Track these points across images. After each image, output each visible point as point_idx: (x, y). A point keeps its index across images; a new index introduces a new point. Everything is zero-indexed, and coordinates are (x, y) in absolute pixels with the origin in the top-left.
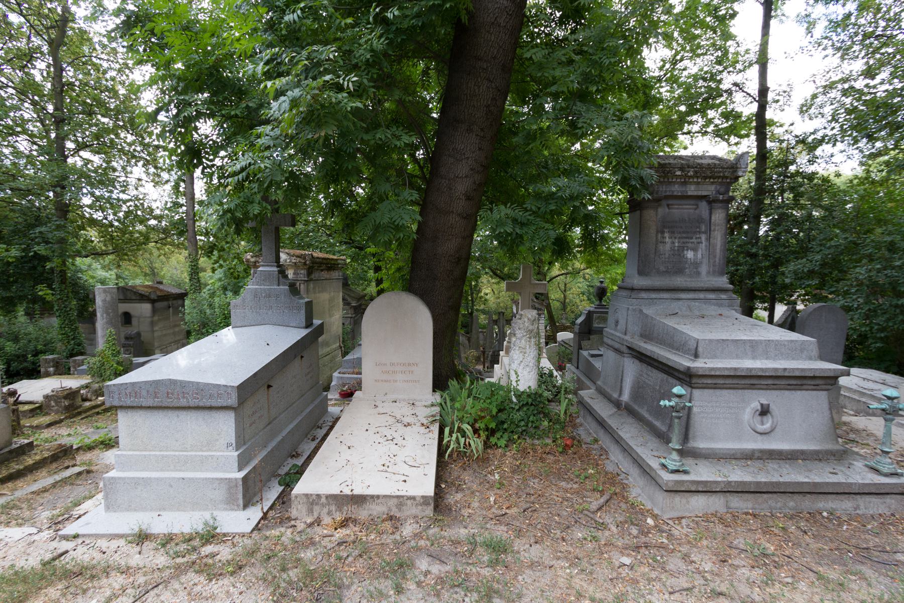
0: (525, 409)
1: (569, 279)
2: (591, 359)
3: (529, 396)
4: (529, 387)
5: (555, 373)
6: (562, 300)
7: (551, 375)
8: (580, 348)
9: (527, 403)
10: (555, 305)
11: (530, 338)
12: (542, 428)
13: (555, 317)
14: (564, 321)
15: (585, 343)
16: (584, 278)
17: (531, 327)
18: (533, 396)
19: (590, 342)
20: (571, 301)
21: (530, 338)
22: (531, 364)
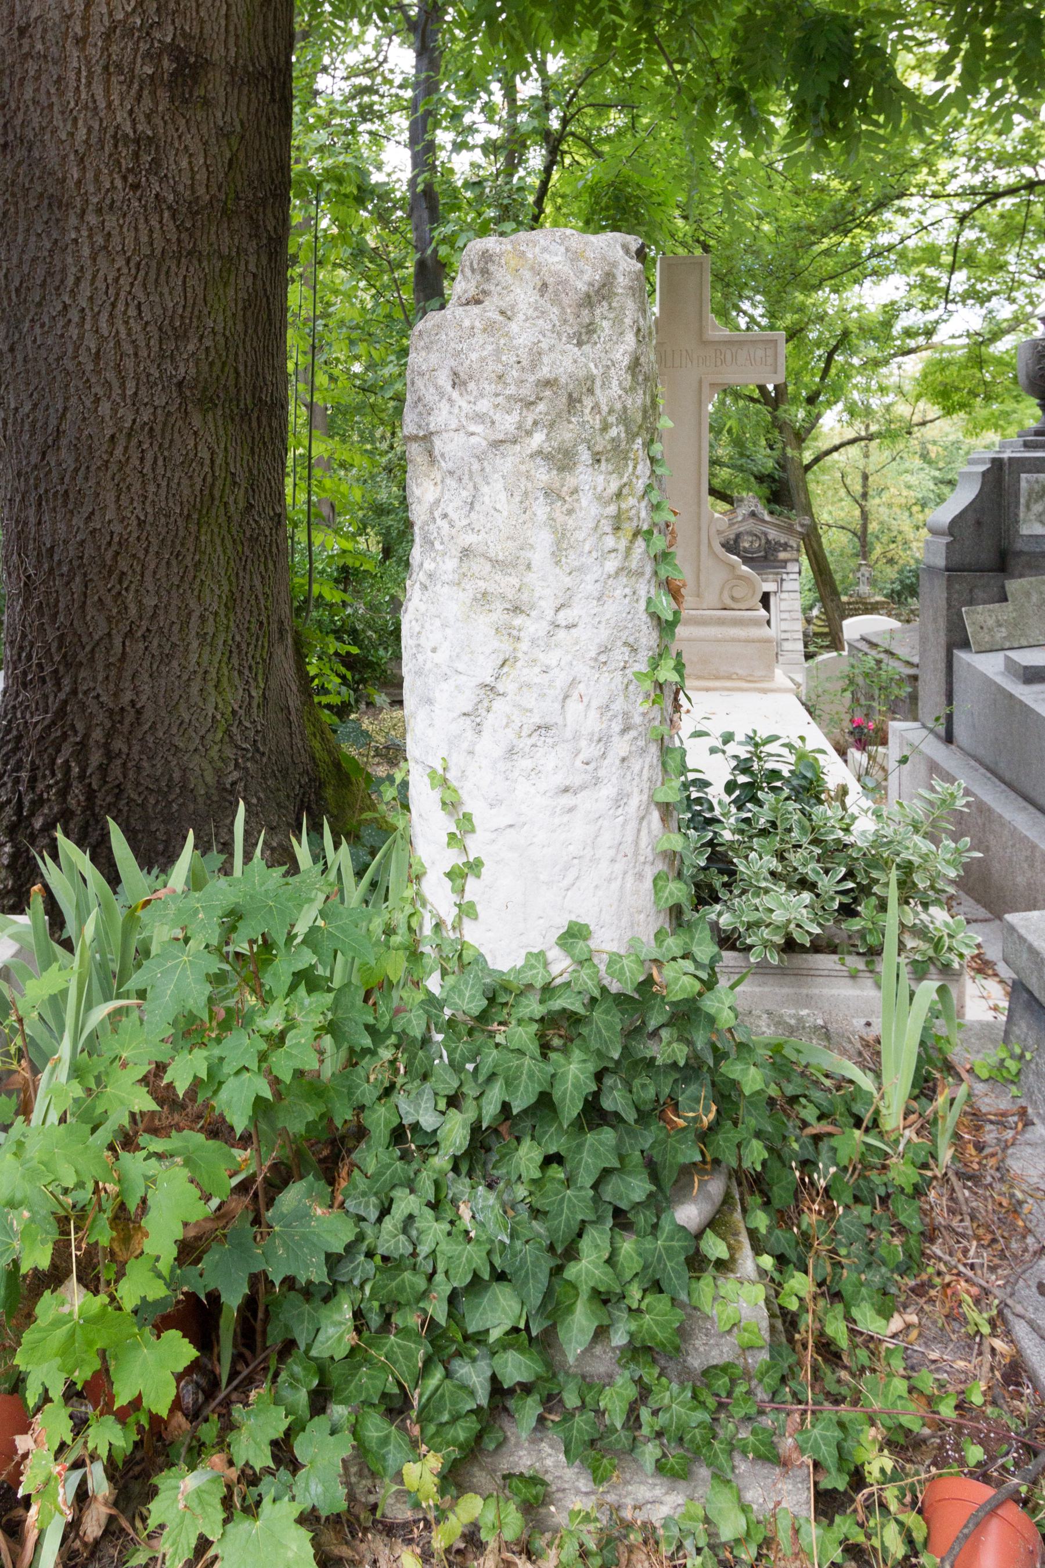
0: (527, 1156)
1: (880, 454)
2: (1026, 694)
3: (559, 1028)
4: (574, 935)
5: (836, 772)
6: (857, 525)
7: (808, 788)
8: (959, 639)
9: (545, 1103)
10: (835, 542)
11: (562, 460)
12: (707, 1352)
13: (837, 577)
14: (864, 589)
15: (979, 618)
16: (924, 456)
17: (565, 362)
18: (606, 1025)
19: (1005, 611)
20: (885, 528)
21: (562, 460)
22: (582, 718)
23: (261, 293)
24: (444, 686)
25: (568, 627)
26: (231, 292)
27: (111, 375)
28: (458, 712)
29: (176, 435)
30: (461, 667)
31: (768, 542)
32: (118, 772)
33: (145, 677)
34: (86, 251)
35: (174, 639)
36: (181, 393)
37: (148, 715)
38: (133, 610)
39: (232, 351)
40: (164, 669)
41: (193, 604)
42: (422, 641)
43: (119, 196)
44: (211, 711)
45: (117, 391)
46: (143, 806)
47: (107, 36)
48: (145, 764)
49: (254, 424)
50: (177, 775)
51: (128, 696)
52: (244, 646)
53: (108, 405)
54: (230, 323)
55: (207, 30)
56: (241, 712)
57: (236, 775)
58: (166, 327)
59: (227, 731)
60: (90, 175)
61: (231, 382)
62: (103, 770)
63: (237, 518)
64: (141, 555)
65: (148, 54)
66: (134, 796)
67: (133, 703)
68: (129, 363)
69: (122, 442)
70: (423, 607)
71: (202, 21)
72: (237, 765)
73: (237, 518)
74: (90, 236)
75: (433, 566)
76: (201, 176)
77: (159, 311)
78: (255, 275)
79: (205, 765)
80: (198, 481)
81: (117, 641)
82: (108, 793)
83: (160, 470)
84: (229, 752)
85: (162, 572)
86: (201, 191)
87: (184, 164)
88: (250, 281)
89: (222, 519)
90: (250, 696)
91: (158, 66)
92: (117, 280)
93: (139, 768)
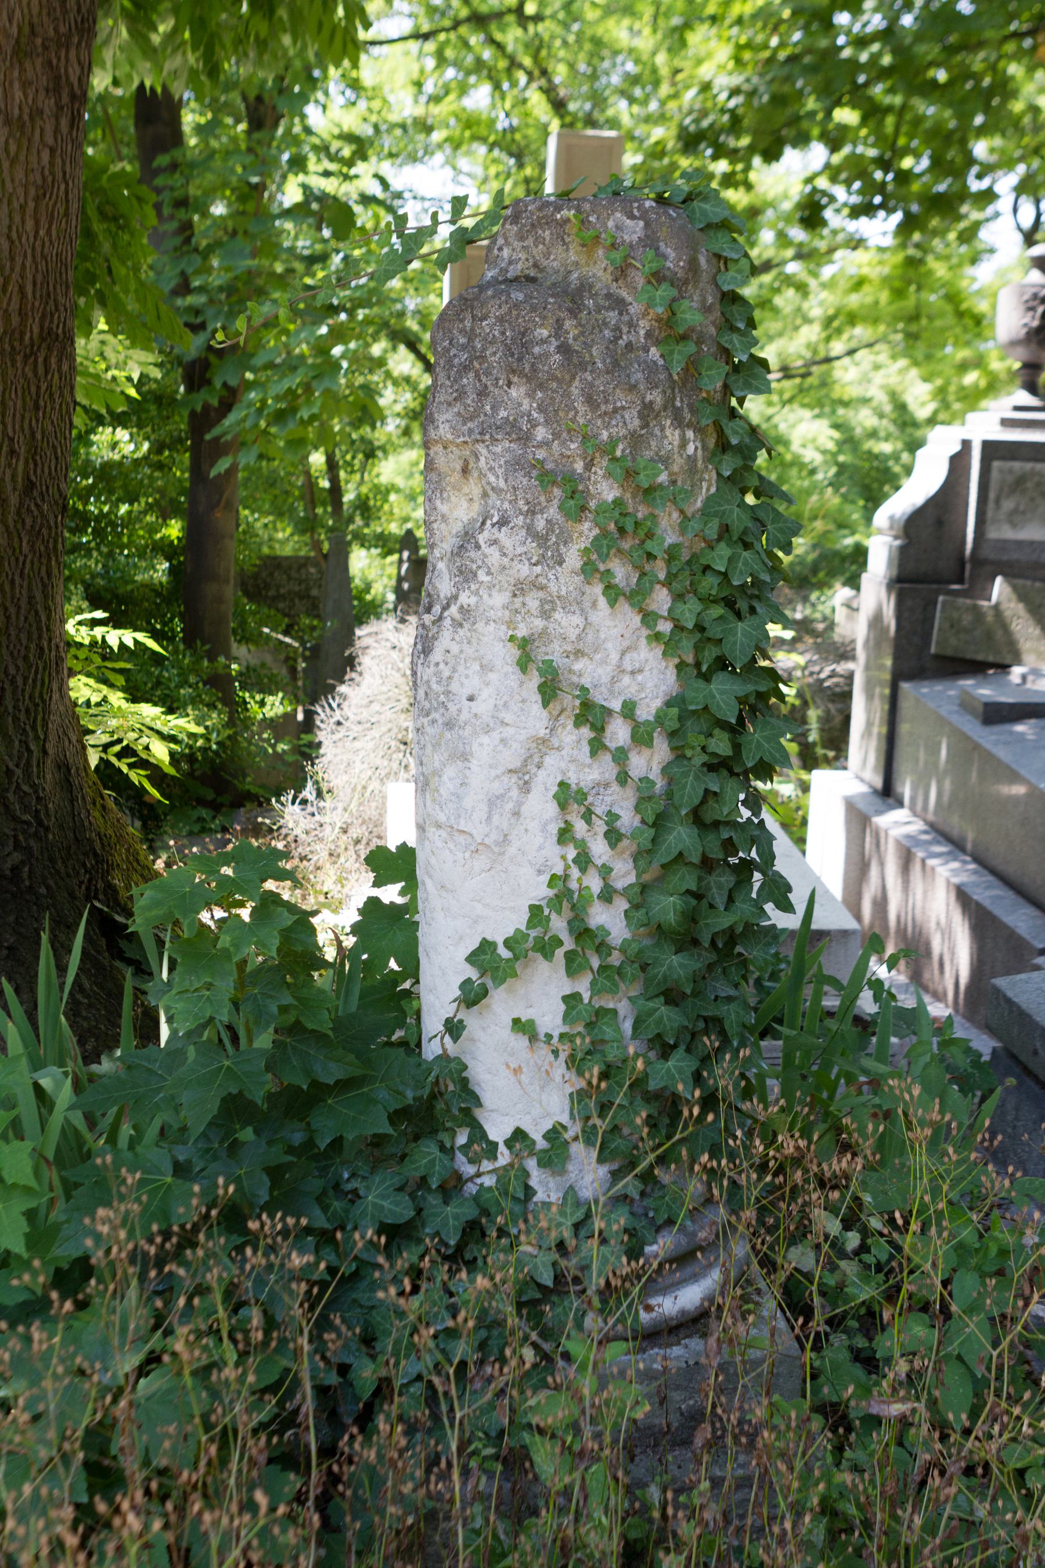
23: (59, 175)
24: (485, 739)
25: (633, 673)
26: (20, 175)
28: (501, 769)
30: (508, 717)
39: (19, 260)
42: (454, 687)
49: (41, 370)
52: (20, 680)
54: (17, 218)
56: (18, 772)
57: (17, 857)
61: (15, 305)
70: (455, 648)
72: (17, 845)
75: (473, 600)
78: (53, 151)
88: (46, 155)
90: (28, 750)
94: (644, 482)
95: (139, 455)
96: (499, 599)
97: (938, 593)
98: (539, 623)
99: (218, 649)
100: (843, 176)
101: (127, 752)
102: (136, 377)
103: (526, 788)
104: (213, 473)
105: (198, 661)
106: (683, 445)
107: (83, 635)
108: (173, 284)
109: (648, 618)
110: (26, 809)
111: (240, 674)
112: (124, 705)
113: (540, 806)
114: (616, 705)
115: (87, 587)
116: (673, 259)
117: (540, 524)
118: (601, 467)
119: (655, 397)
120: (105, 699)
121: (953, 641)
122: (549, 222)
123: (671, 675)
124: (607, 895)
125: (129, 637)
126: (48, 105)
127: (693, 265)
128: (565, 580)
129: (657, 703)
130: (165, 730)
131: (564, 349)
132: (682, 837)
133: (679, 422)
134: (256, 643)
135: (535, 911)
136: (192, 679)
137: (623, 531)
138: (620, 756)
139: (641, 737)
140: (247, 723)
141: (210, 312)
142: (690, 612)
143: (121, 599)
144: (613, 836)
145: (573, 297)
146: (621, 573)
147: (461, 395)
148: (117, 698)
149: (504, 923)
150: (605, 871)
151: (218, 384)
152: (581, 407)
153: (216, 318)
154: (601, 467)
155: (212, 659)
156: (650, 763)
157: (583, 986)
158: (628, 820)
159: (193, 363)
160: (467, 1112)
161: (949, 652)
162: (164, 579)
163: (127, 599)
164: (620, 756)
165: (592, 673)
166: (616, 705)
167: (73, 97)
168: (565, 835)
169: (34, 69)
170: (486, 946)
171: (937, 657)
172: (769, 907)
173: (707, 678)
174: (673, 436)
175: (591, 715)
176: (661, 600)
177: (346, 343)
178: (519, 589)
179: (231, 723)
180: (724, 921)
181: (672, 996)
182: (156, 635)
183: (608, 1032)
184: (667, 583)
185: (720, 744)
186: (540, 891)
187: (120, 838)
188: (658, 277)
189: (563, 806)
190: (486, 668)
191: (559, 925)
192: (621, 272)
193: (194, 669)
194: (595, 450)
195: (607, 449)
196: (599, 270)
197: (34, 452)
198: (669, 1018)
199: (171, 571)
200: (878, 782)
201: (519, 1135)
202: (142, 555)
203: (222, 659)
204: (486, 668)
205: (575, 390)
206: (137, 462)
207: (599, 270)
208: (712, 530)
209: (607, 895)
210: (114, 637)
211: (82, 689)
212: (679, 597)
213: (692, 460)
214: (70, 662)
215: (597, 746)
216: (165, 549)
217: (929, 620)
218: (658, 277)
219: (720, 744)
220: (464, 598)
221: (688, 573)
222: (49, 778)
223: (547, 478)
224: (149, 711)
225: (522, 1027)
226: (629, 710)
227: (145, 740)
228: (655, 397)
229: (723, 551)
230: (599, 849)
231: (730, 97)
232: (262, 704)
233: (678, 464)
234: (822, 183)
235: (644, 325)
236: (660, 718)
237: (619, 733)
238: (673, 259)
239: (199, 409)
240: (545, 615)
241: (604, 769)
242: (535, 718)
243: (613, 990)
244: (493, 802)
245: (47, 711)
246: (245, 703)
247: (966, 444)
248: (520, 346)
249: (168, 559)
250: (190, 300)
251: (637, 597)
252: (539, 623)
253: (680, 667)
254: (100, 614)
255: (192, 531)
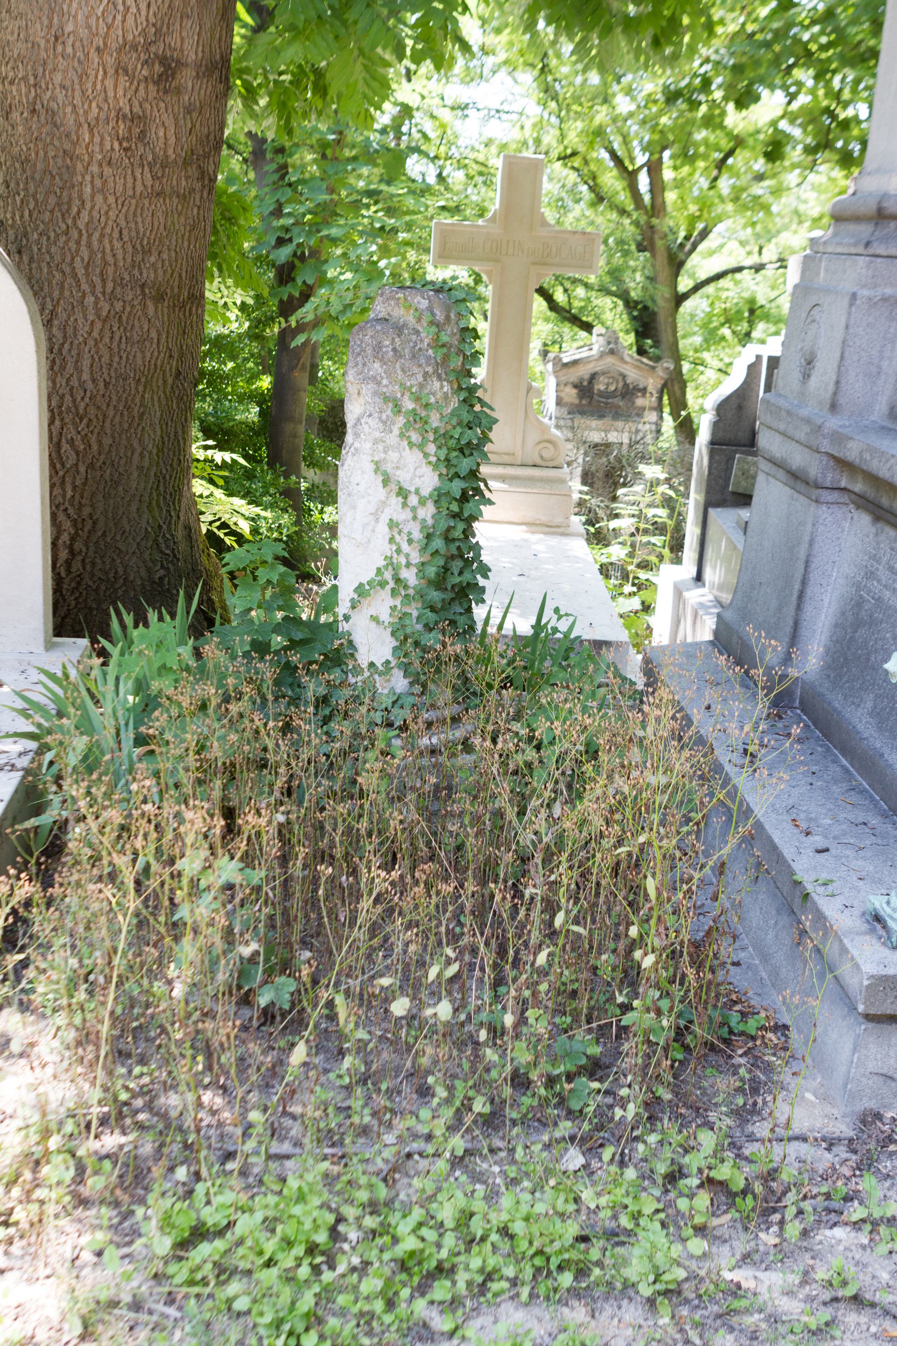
26: (182, 220)
27: (97, 280)
29: (136, 323)
31: (626, 385)
32: (80, 565)
33: (100, 497)
34: (88, 190)
35: (121, 470)
36: (143, 292)
37: (101, 525)
38: (95, 447)
40: (113, 492)
41: (136, 444)
43: (116, 155)
44: (144, 525)
45: (99, 289)
46: (96, 591)
47: (119, 51)
48: (98, 560)
50: (121, 571)
51: (86, 511)
53: (92, 299)
55: (185, 46)
57: (162, 572)
58: (138, 246)
59: (156, 541)
60: (97, 139)
62: (68, 563)
63: (170, 381)
64: (104, 407)
65: (146, 62)
66: (90, 583)
67: (91, 516)
68: (110, 270)
69: (98, 325)
71: (182, 39)
72: (162, 567)
73: (170, 381)
74: (92, 182)
76: (172, 141)
77: (133, 234)
79: (141, 564)
80: (148, 355)
81: (82, 469)
82: (72, 580)
83: (123, 346)
84: (157, 556)
85: (117, 419)
86: (170, 151)
87: (161, 134)
88: (195, 211)
89: (161, 382)
91: (151, 70)
92: (107, 213)
93: (93, 564)
94: (424, 402)
95: (241, 331)
96: (368, 446)
97: (736, 452)
98: (383, 456)
99: (291, 469)
100: (799, 121)
101: (224, 525)
102: (239, 303)
103: (377, 520)
104: (293, 345)
105: (277, 478)
106: (442, 387)
107: (201, 455)
108: (271, 208)
109: (426, 455)
110: (168, 547)
111: (308, 489)
112: (224, 497)
113: (383, 529)
114: (413, 489)
115: (202, 422)
116: (440, 316)
117: (384, 417)
118: (406, 397)
119: (430, 369)
120: (211, 495)
121: (744, 483)
122: (393, 298)
123: (436, 478)
124: (408, 565)
125: (228, 456)
126: (198, 186)
127: (448, 318)
128: (393, 438)
129: (430, 489)
130: (247, 514)
131: (394, 350)
132: (438, 543)
133: (439, 378)
134: (321, 468)
135: (379, 570)
136: (272, 491)
137: (417, 420)
138: (414, 509)
139: (422, 502)
140: (311, 525)
141: (296, 230)
142: (443, 453)
143: (226, 432)
144: (410, 541)
145: (399, 329)
146: (415, 437)
147: (357, 365)
148: (219, 493)
149: (367, 575)
150: (407, 556)
151: (299, 282)
152: (399, 372)
153: (299, 235)
154: (407, 394)
155: (287, 477)
156: (428, 512)
157: (398, 602)
158: (417, 535)
159: (283, 266)
160: (352, 655)
161: (741, 491)
162: (256, 419)
163: (228, 432)
164: (414, 509)
165: (404, 477)
166: (413, 489)
167: (210, 180)
168: (392, 540)
169: (193, 171)
170: (361, 585)
171: (734, 493)
172: (478, 577)
173: (451, 480)
174: (437, 384)
175: (403, 493)
176: (431, 448)
177: (389, 258)
178: (376, 442)
179: (297, 523)
180: (457, 580)
181: (433, 609)
182: (246, 457)
183: (407, 622)
184: (434, 442)
185: (455, 507)
186: (382, 563)
187: (217, 574)
188: (432, 323)
189: (391, 528)
190: (363, 472)
191: (388, 575)
192: (419, 320)
193: (273, 484)
194: (405, 389)
195: (409, 389)
196: (411, 319)
197: (182, 355)
198: (431, 617)
199: (261, 414)
200: (694, 574)
201: (372, 665)
202: (241, 402)
203: (293, 478)
204: (363, 472)
205: (398, 366)
206: (240, 336)
207: (411, 319)
208: (454, 421)
209: (408, 565)
210: (219, 456)
211: (199, 487)
212: (439, 447)
213: (446, 394)
214: (194, 470)
215: (405, 505)
216: (260, 399)
217: (728, 470)
218: (432, 323)
219: (455, 507)
220: (356, 445)
221: (441, 438)
222: (180, 534)
223: (386, 399)
224: (238, 503)
225: (375, 619)
226: (417, 492)
227: (234, 519)
228: (430, 369)
229: (459, 430)
230: (405, 547)
231: (701, 65)
232: (321, 512)
233: (439, 395)
234: (783, 125)
235: (426, 341)
236: (431, 496)
237: (413, 500)
238: (440, 316)
239: (285, 298)
240: (385, 452)
241: (407, 515)
242: (381, 493)
243: (409, 604)
244: (364, 526)
245: (181, 495)
246: (310, 510)
247: (759, 358)
248: (378, 347)
249: (259, 404)
250: (282, 222)
251: (421, 447)
252: (383, 456)
253: (440, 475)
254: (210, 442)
255: (280, 385)
